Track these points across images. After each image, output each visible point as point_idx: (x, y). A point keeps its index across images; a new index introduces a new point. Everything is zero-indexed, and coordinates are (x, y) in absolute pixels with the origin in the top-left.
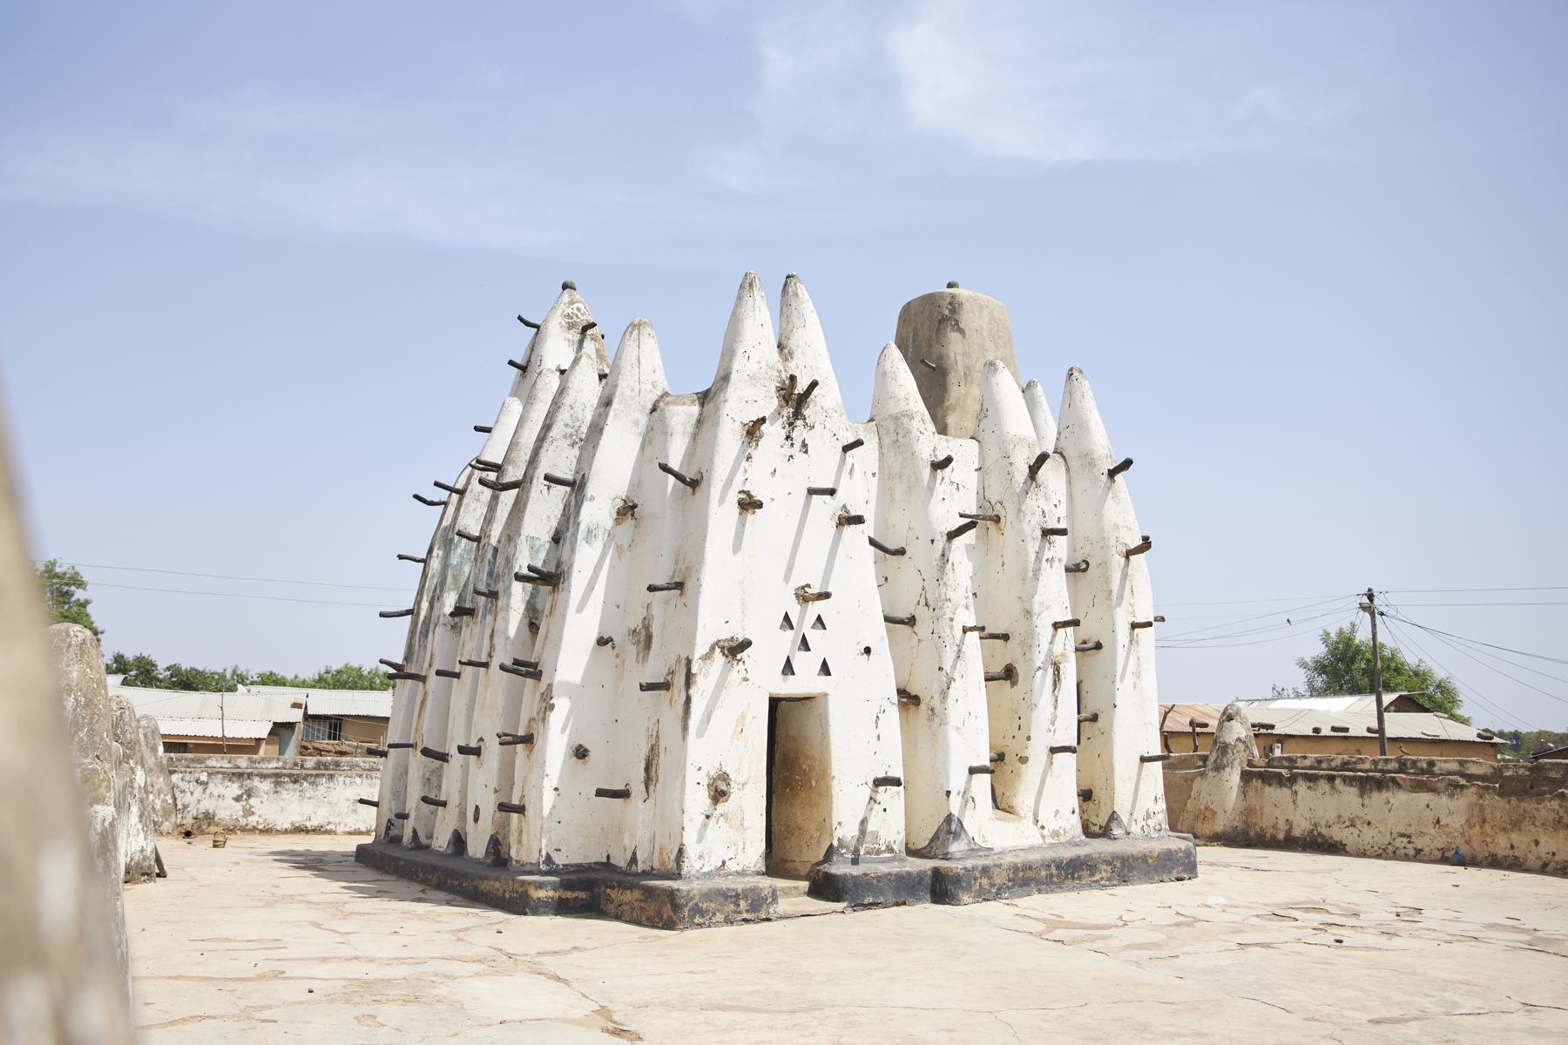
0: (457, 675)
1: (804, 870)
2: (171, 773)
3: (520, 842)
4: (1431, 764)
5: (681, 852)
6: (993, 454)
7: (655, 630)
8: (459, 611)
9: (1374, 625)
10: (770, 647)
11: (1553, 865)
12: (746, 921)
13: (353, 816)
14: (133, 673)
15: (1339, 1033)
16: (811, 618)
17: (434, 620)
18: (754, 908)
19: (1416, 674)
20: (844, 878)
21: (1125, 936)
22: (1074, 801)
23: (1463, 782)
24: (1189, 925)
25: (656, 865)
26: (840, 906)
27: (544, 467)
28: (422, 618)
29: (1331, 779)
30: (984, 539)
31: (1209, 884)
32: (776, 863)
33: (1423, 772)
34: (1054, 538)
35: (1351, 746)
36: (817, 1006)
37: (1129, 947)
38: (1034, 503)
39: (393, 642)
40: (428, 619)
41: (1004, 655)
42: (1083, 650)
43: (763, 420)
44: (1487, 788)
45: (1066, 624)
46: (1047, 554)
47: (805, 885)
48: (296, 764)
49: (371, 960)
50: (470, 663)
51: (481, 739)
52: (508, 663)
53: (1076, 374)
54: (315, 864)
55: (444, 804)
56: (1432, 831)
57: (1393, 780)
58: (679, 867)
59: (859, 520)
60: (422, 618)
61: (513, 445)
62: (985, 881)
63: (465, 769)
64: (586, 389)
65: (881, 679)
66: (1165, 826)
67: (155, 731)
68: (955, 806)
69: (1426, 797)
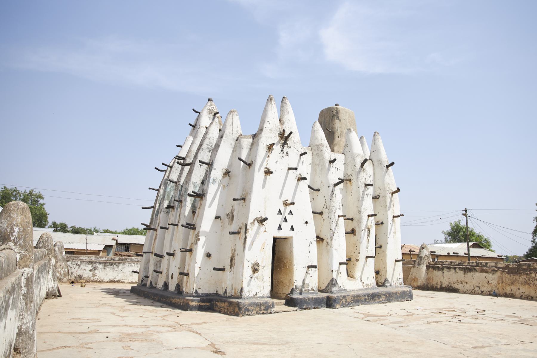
0: (167, 229)
1: (284, 297)
2: (68, 261)
3: (186, 286)
4: (487, 264)
5: (242, 289)
6: (349, 159)
7: (235, 214)
8: (169, 207)
9: (467, 220)
10: (274, 220)
11: (524, 296)
12: (263, 313)
13: (131, 277)
14: (59, 228)
15: (463, 352)
16: (288, 211)
17: (160, 210)
18: (266, 309)
19: (478, 236)
20: (297, 299)
21: (391, 319)
22: (374, 274)
23: (496, 269)
24: (411, 315)
25: (233, 294)
26: (295, 309)
27: (200, 158)
28: (156, 209)
29: (455, 268)
30: (346, 187)
31: (417, 302)
32: (274, 294)
33: (484, 266)
34: (369, 187)
35: (459, 258)
36: (287, 343)
37: (392, 323)
38: (362, 175)
39: (146, 217)
40: (158, 210)
41: (352, 225)
42: (377, 224)
43: (274, 144)
44: (504, 271)
45: (372, 215)
46: (366, 192)
47: (284, 301)
48: (112, 259)
49: (131, 326)
50: (172, 224)
51: (175, 250)
52: (185, 224)
53: (377, 134)
54: (116, 293)
55: (161, 273)
56: (487, 285)
57: (475, 269)
58: (241, 295)
59: (305, 179)
60: (156, 209)
61: (189, 151)
62: (344, 301)
63: (169, 260)
64: (214, 133)
65: (311, 232)
66: (403, 283)
67: (62, 246)
68: (334, 275)
69: (485, 274)
